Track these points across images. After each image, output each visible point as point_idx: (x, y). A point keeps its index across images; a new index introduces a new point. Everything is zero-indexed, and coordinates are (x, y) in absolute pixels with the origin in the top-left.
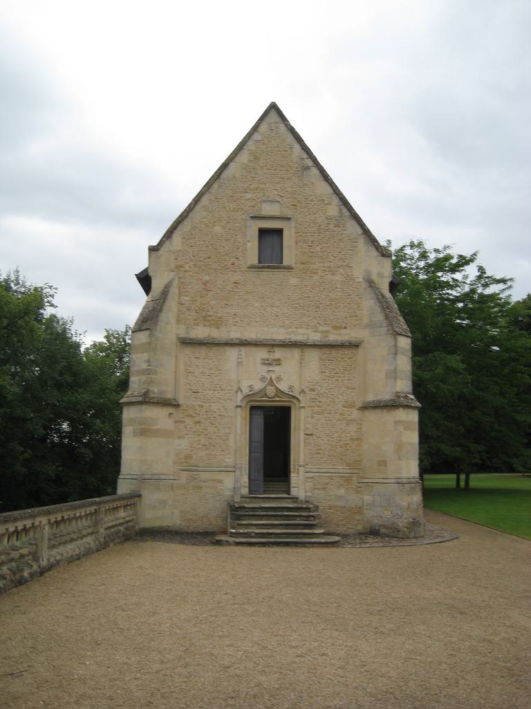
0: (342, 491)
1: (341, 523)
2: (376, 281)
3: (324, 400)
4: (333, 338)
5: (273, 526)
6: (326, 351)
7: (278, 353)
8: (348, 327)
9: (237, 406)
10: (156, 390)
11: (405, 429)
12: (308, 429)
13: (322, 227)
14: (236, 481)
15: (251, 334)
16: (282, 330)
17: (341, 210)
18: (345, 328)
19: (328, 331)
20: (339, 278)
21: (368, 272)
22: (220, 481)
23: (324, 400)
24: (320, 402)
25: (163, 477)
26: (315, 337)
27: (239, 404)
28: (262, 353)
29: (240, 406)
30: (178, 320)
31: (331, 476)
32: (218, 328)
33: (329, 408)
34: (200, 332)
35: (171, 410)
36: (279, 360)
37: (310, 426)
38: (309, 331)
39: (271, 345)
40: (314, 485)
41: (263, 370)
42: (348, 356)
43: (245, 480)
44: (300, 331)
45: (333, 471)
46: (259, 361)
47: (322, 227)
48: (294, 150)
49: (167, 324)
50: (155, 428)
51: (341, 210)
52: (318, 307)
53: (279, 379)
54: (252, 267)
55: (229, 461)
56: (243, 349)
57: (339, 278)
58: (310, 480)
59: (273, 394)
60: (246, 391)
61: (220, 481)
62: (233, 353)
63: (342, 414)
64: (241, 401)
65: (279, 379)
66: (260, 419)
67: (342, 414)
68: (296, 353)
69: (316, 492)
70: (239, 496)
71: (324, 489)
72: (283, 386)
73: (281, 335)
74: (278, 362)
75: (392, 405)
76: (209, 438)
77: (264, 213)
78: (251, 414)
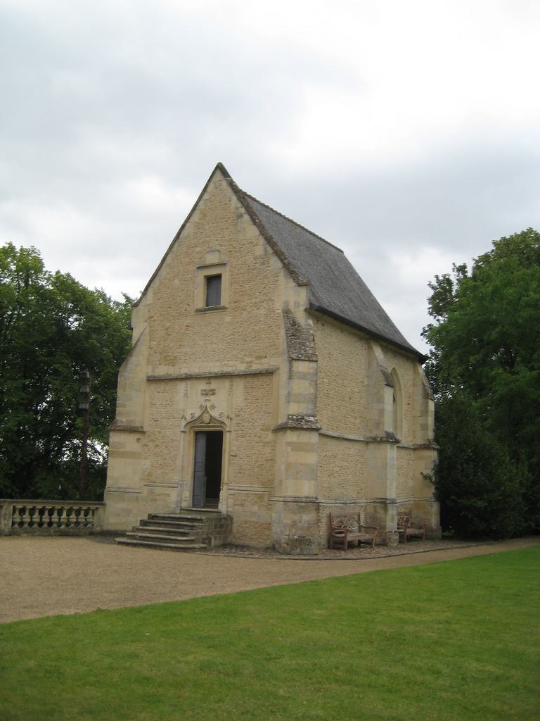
0: (255, 508)
2: (293, 311)
3: (246, 424)
6: (249, 379)
7: (214, 385)
9: (182, 432)
10: (124, 420)
12: (233, 451)
14: (180, 495)
15: (195, 369)
16: (218, 364)
18: (266, 357)
21: (287, 303)
22: (168, 495)
23: (246, 424)
24: (243, 426)
25: (128, 490)
26: (241, 368)
27: (183, 429)
28: (202, 386)
29: (184, 432)
30: (148, 362)
31: (246, 494)
33: (251, 431)
34: (162, 371)
35: (138, 436)
36: (213, 390)
37: (235, 448)
38: (237, 363)
39: (209, 378)
40: (235, 501)
41: (202, 399)
43: (187, 494)
44: (231, 363)
45: (250, 489)
46: (200, 392)
48: (232, 202)
52: (246, 340)
53: (213, 407)
54: (198, 311)
55: (176, 478)
56: (189, 382)
57: (262, 311)
58: (232, 497)
59: (208, 421)
60: (189, 418)
62: (181, 386)
63: (259, 437)
65: (213, 407)
66: (202, 442)
67: (259, 437)
68: (227, 383)
69: (236, 507)
70: (179, 509)
71: (242, 505)
72: (215, 414)
73: (216, 368)
74: (213, 392)
76: (164, 459)
77: (208, 262)
78: (196, 439)
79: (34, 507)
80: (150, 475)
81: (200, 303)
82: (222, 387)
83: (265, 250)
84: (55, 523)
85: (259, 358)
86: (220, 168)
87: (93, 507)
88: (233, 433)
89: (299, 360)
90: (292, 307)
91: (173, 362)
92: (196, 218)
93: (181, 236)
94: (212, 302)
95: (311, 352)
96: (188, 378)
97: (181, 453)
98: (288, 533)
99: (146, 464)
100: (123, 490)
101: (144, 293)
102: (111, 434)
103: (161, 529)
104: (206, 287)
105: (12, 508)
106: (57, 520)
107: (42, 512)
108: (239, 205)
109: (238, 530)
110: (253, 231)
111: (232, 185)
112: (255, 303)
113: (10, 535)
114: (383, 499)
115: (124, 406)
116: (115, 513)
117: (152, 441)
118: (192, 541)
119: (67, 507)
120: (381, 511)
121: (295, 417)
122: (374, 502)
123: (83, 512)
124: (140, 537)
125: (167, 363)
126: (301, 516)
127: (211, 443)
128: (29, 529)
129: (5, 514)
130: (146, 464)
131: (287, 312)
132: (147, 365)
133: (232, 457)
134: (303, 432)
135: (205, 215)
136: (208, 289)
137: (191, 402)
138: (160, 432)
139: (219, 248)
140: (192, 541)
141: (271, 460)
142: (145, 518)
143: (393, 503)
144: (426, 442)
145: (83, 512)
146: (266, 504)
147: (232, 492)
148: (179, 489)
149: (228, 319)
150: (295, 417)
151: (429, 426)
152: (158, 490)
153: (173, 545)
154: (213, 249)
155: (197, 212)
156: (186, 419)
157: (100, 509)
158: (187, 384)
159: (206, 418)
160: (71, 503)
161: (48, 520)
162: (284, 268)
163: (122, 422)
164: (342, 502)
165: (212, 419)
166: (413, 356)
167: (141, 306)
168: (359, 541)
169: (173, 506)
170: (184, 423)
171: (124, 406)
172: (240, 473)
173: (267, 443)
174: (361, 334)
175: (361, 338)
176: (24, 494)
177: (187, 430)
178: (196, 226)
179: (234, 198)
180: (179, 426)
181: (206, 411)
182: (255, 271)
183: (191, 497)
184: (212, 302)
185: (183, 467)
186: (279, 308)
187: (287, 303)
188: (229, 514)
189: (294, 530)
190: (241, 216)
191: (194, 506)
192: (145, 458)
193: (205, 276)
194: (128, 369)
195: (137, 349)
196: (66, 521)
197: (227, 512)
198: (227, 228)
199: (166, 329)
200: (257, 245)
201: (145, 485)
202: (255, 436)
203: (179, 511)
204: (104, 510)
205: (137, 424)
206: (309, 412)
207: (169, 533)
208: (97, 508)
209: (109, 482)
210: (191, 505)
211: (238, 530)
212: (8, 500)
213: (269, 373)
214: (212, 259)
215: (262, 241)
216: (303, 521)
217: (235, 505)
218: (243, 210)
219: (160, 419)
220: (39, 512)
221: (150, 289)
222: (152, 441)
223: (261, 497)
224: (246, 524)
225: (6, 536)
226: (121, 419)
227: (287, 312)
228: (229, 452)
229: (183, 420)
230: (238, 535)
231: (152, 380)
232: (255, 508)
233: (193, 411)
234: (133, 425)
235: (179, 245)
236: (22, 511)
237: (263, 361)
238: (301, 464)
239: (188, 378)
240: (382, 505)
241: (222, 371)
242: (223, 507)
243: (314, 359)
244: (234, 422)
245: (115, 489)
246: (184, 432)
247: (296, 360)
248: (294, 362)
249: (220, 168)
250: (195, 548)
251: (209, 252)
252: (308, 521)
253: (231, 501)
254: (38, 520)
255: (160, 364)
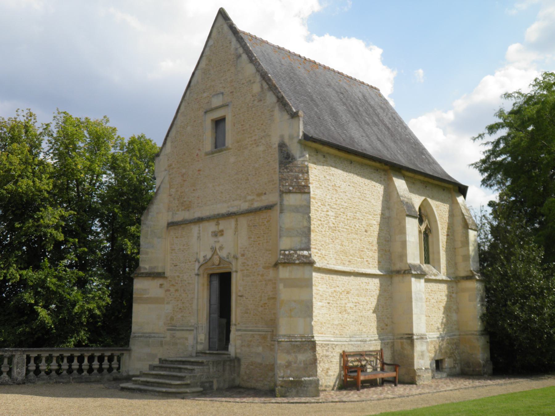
0: (260, 349)
1: (259, 379)
2: (288, 144)
4: (256, 205)
5: (170, 385)
7: (223, 224)
8: (267, 193)
10: (147, 267)
11: (285, 286)
12: (240, 291)
13: (250, 105)
14: (196, 338)
17: (262, 85)
18: (265, 194)
19: (254, 199)
20: (261, 148)
21: (282, 137)
25: (153, 335)
26: (245, 206)
28: (211, 227)
30: (169, 209)
31: (253, 335)
32: (188, 210)
34: (180, 216)
35: (160, 281)
41: (211, 241)
42: (266, 220)
43: (202, 337)
47: (250, 105)
48: (232, 43)
49: (157, 213)
50: (145, 296)
51: (262, 85)
52: (248, 179)
54: (207, 154)
55: (193, 321)
57: (261, 148)
61: (187, 339)
62: (195, 229)
63: (262, 275)
64: (199, 269)
66: (216, 283)
67: (262, 275)
68: (232, 222)
73: (223, 209)
74: (221, 233)
75: (469, 278)
77: (214, 106)
78: (210, 282)
79: (61, 355)
80: (172, 319)
81: (208, 145)
82: (228, 225)
83: (262, 87)
84: (75, 369)
85: (259, 195)
86: (222, 14)
87: (117, 353)
88: (239, 274)
89: (290, 192)
90: (287, 141)
91: (187, 207)
92: (203, 65)
93: (192, 84)
94: (219, 144)
95: (303, 183)
96: (200, 220)
97: (196, 297)
98: (282, 375)
99: (168, 308)
100: (147, 335)
101: (165, 143)
102: (135, 281)
103: (162, 373)
104: (214, 131)
105: (25, 356)
106: (78, 367)
107: (101, 359)
108: (238, 46)
109: (245, 373)
110: (250, 69)
111: (232, 28)
112: (255, 140)
113: (24, 383)
114: (409, 334)
115: (147, 253)
116: (138, 359)
117: (173, 285)
118: (187, 385)
119: (45, 355)
120: (407, 347)
121: (287, 252)
122: (402, 338)
123: (106, 358)
124: (142, 381)
125: (183, 208)
126: (296, 357)
127: (223, 282)
128: (46, 377)
129: (18, 363)
130: (168, 308)
131: (282, 146)
132: (168, 211)
133: (239, 298)
134: (295, 267)
135: (210, 61)
136: (216, 132)
137: (201, 244)
138: (178, 277)
139: (222, 90)
140: (187, 385)
141: (273, 298)
142: (156, 362)
143: (422, 338)
144: (469, 274)
145: (106, 358)
146: (269, 345)
147: (240, 333)
148: (195, 332)
149: (232, 160)
150: (287, 252)
151: (471, 257)
152: (178, 334)
153: (164, 390)
154: (218, 93)
155: (204, 58)
156: (199, 262)
157: (125, 355)
158: (199, 227)
159: (216, 260)
160: (92, 350)
161: (117, 366)
162: (278, 101)
163: (145, 269)
164: (361, 339)
165: (221, 259)
166: (451, 186)
167: (162, 157)
168: (382, 379)
169: (190, 349)
170: (197, 266)
171: (147, 253)
172: (247, 313)
173: (270, 280)
174: (377, 165)
175: (377, 169)
176: (5, 344)
177: (201, 272)
178: (204, 73)
179: (234, 40)
180: (194, 270)
181: (214, 251)
182: (254, 109)
183: (207, 340)
184: (219, 144)
185: (197, 310)
186: (275, 141)
187: (282, 137)
188: (238, 355)
189: (289, 371)
190: (239, 56)
191: (210, 349)
192: (168, 303)
193: (212, 120)
194: (149, 217)
195: (159, 197)
196: (87, 367)
197: (236, 353)
198: (229, 70)
199: (182, 176)
200: (254, 82)
201: (168, 330)
202: (258, 274)
203: (194, 354)
204: (130, 356)
205: (160, 270)
206: (303, 246)
207: (156, 376)
208: (123, 354)
209: (134, 328)
210: (207, 347)
211: (245, 373)
212: (20, 349)
213: (269, 208)
214: (217, 102)
215: (258, 78)
216: (298, 362)
217: (242, 346)
218: (241, 50)
219: (178, 264)
220: (67, 359)
221: (169, 139)
222: (173, 285)
223: (264, 338)
224: (252, 365)
225: (19, 384)
226: (145, 266)
227: (282, 146)
228: (236, 293)
229: (197, 263)
230: (245, 378)
231: (171, 225)
232: (260, 349)
233: (205, 253)
234: (156, 271)
235: (190, 93)
236: (61, 358)
237: (263, 197)
238: (295, 301)
239: (200, 220)
240: (409, 341)
241: (229, 211)
242: (232, 349)
243: (306, 191)
244: (240, 261)
245: (140, 335)
246: (198, 275)
247: (286, 193)
248: (284, 195)
249: (222, 14)
250: (186, 393)
251: (214, 95)
252: (304, 361)
253: (239, 342)
254: (67, 367)
255: (178, 210)
